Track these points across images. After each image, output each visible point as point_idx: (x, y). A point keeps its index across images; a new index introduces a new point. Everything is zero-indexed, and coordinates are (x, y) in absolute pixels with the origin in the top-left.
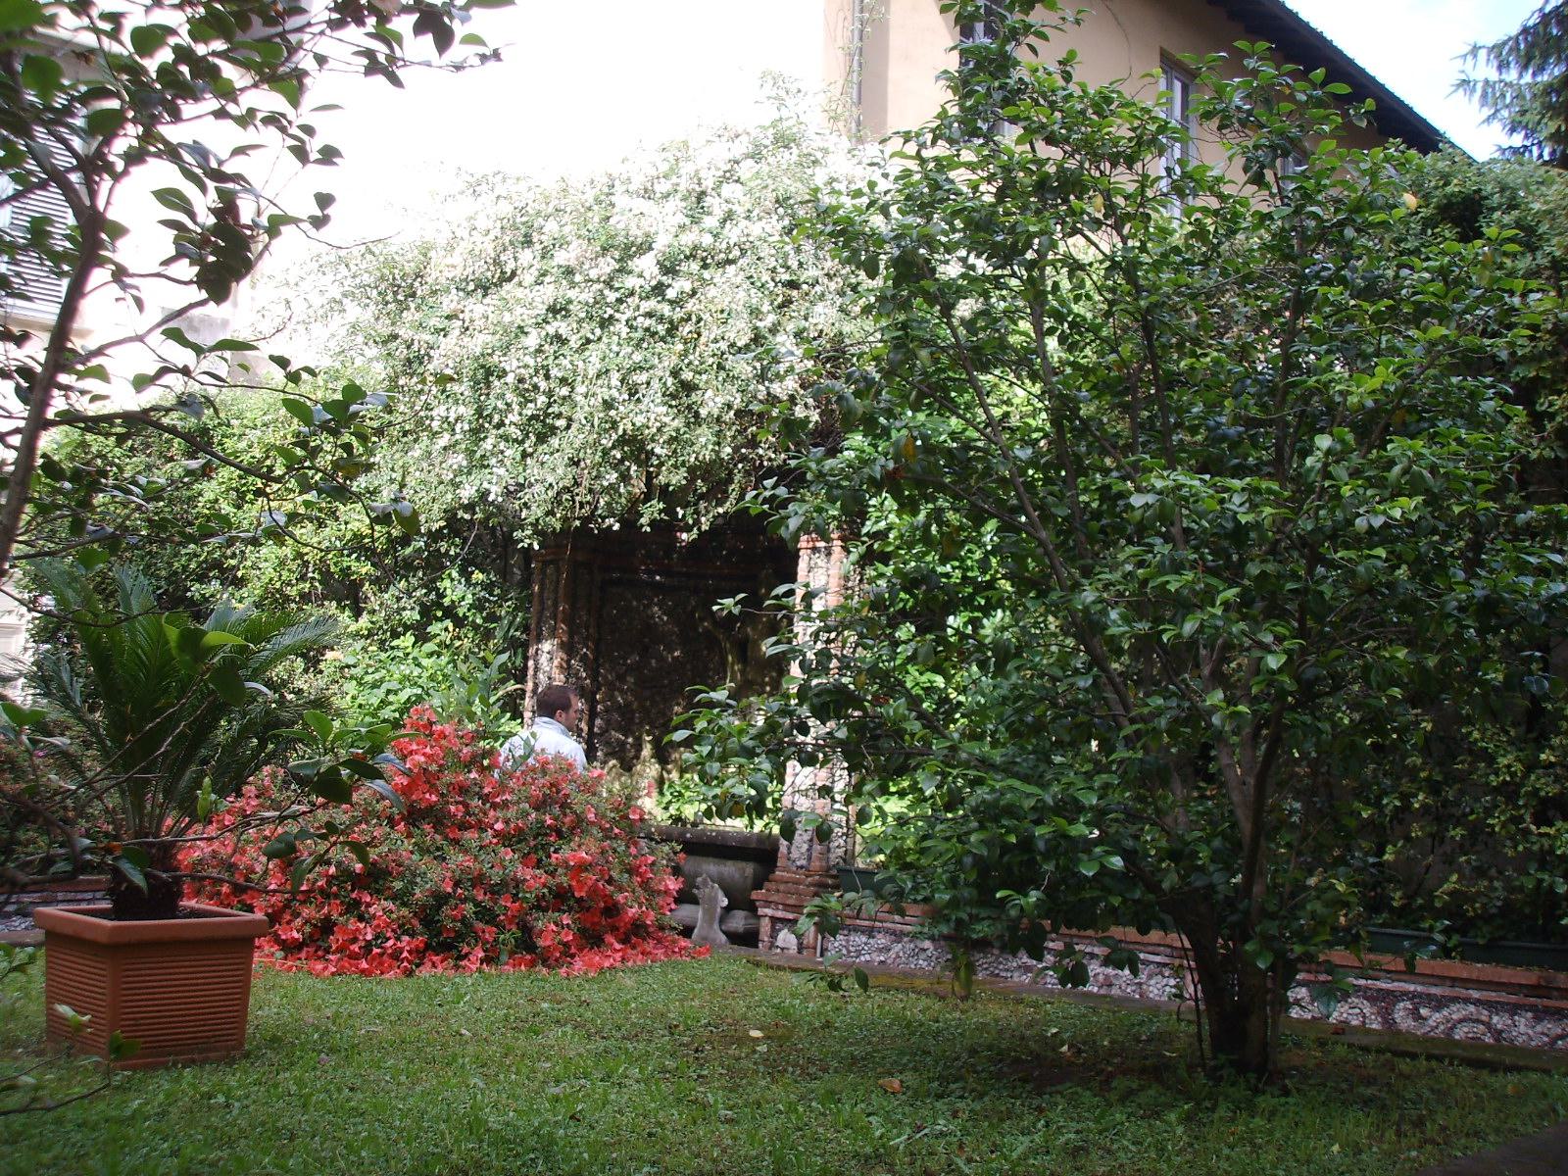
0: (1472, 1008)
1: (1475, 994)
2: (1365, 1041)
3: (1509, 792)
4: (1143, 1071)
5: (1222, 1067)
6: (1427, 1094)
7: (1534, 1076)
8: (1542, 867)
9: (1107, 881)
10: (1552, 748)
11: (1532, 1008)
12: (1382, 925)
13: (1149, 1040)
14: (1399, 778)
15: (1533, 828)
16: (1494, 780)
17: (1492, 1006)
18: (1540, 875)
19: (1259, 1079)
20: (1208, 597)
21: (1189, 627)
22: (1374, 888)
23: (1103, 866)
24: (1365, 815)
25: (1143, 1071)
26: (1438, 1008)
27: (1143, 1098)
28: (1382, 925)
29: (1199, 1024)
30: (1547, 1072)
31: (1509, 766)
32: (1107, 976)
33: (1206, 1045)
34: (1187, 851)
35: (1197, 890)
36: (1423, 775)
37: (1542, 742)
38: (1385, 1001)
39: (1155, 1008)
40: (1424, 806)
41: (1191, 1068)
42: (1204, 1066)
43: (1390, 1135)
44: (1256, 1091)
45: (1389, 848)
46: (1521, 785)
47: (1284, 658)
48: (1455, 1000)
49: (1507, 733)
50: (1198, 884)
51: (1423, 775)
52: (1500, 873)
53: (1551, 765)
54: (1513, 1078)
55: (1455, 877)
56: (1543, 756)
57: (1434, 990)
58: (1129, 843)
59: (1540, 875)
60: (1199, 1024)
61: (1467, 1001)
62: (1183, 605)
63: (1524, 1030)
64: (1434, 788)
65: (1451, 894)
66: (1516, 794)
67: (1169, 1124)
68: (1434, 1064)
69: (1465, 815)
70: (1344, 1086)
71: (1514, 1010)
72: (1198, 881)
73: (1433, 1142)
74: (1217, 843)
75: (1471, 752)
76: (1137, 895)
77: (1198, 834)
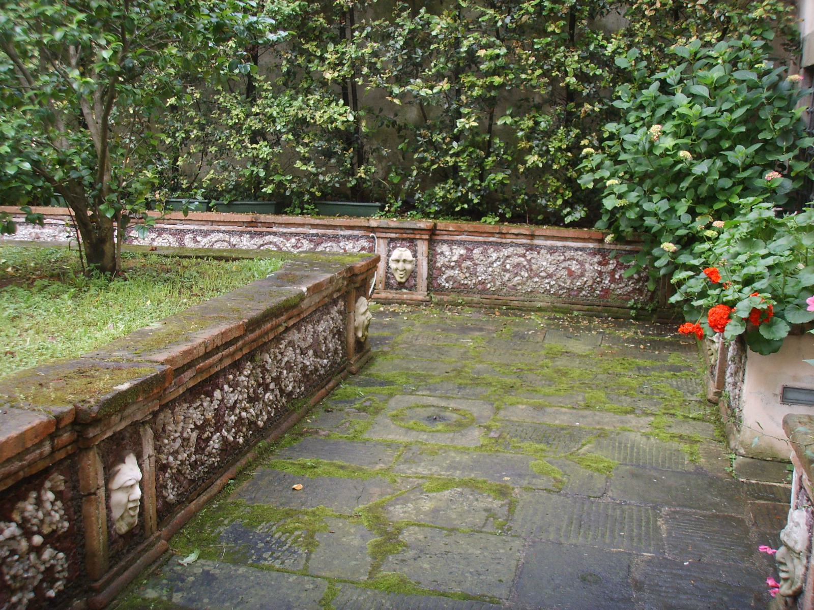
0: (221, 235)
1: (223, 228)
2: (166, 253)
3: (238, 127)
4: (52, 276)
5: (92, 270)
6: (195, 274)
7: (246, 262)
8: (254, 164)
9: (24, 177)
10: (258, 105)
11: (249, 232)
12: (178, 197)
13: (56, 262)
14: (183, 123)
15: (249, 145)
16: (230, 123)
17: (230, 233)
18: (252, 168)
19: (112, 275)
20: (69, 17)
21: (58, 35)
22: (173, 180)
23: (19, 168)
24: (167, 142)
25: (52, 276)
26: (205, 236)
27: (50, 289)
28: (178, 197)
29: (80, 251)
30: (252, 259)
31: (237, 115)
32: (37, 234)
33: (85, 260)
34: (68, 160)
35: (74, 179)
36: (196, 120)
37: (253, 103)
38: (180, 234)
39: (59, 246)
40: (197, 136)
41: (76, 273)
42: (83, 271)
43: (176, 294)
44: (110, 280)
45: (180, 159)
46: (243, 124)
47: (111, 52)
48: (213, 231)
49: (236, 98)
50: (74, 176)
51: (196, 120)
52: (234, 168)
53: (257, 114)
54: (236, 263)
55: (212, 172)
56: (253, 110)
57: (203, 228)
58: (36, 157)
59: (252, 168)
60: (80, 251)
61: (219, 231)
62: (55, 23)
63: (246, 243)
64: (202, 128)
65: (210, 180)
66: (241, 128)
67: (63, 300)
68: (199, 260)
69: (217, 140)
70: (155, 274)
71: (241, 234)
72: (74, 175)
73: (196, 295)
74: (85, 155)
75: (219, 108)
76: (41, 183)
77: (74, 150)
